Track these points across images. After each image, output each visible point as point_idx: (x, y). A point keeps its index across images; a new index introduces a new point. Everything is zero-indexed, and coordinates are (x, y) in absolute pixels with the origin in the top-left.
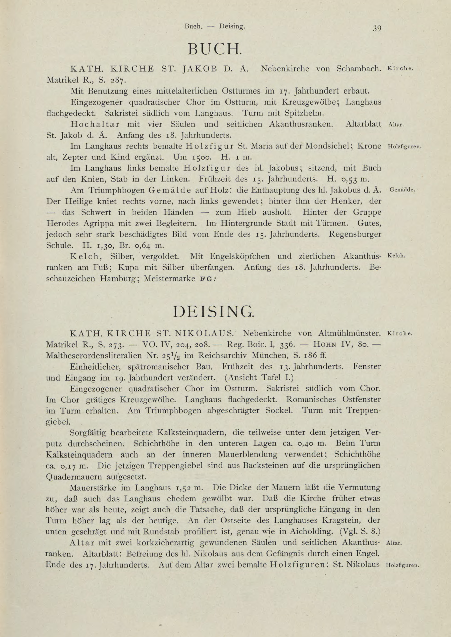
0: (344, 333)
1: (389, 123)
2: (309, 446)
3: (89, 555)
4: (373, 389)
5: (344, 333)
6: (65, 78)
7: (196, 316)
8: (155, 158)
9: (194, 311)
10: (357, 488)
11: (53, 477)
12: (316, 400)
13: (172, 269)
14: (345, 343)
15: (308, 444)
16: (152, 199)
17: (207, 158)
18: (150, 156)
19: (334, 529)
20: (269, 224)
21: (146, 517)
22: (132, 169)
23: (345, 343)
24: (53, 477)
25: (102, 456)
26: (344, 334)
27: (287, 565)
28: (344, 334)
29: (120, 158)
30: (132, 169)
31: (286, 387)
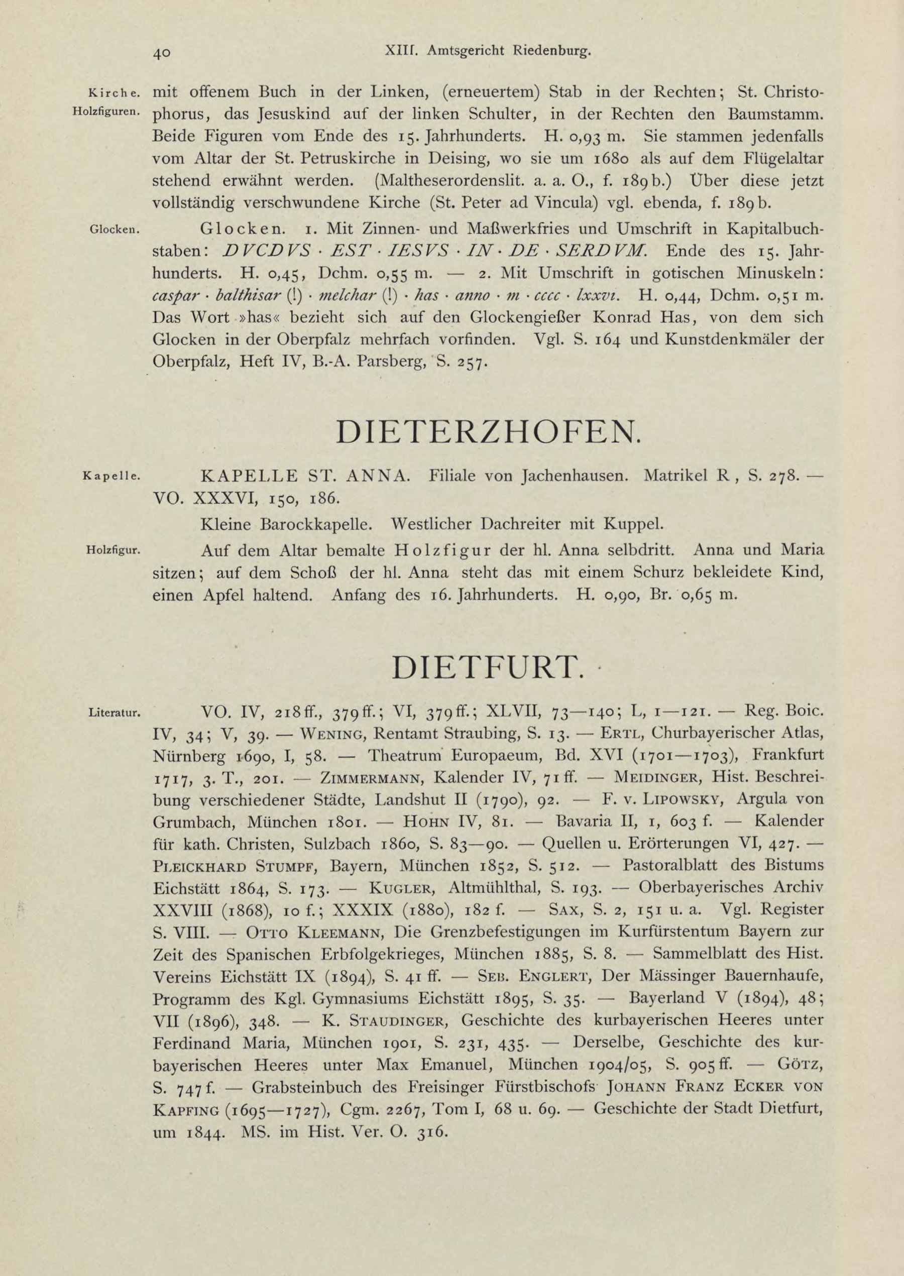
0: (500, 888)
1: (349, 472)
2: (162, 57)
3: (206, 160)
4: (176, 115)
5: (500, 888)
6: (681, 472)
7: (398, 441)
8: (469, 933)
9: (393, 431)
10: (801, 115)
11: (556, 844)
12: (268, 956)
13: (683, 868)
14: (465, 819)
15: (161, 54)
16: (714, 314)
17: (499, 845)
18: (200, 200)
19: (215, 147)
20: (190, 137)
21: (200, 145)
22: (422, 116)
23: (465, 818)
24: (556, 844)
25: (697, 1111)
26: (500, 890)
27: (431, 552)
28: (500, 890)
29: (800, 574)
30: (422, 116)
31: (796, 89)
